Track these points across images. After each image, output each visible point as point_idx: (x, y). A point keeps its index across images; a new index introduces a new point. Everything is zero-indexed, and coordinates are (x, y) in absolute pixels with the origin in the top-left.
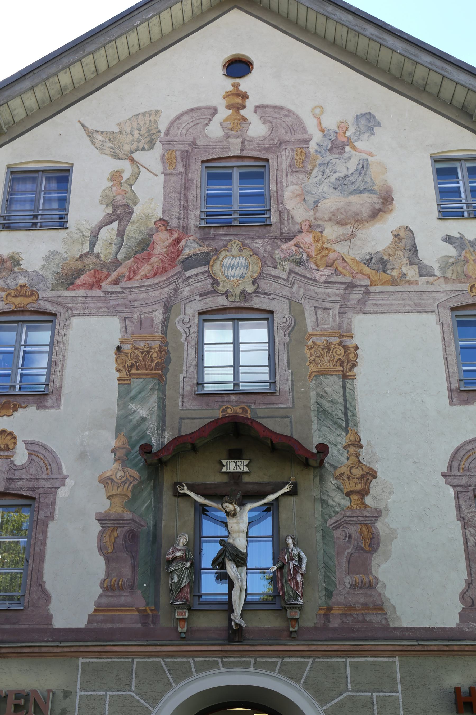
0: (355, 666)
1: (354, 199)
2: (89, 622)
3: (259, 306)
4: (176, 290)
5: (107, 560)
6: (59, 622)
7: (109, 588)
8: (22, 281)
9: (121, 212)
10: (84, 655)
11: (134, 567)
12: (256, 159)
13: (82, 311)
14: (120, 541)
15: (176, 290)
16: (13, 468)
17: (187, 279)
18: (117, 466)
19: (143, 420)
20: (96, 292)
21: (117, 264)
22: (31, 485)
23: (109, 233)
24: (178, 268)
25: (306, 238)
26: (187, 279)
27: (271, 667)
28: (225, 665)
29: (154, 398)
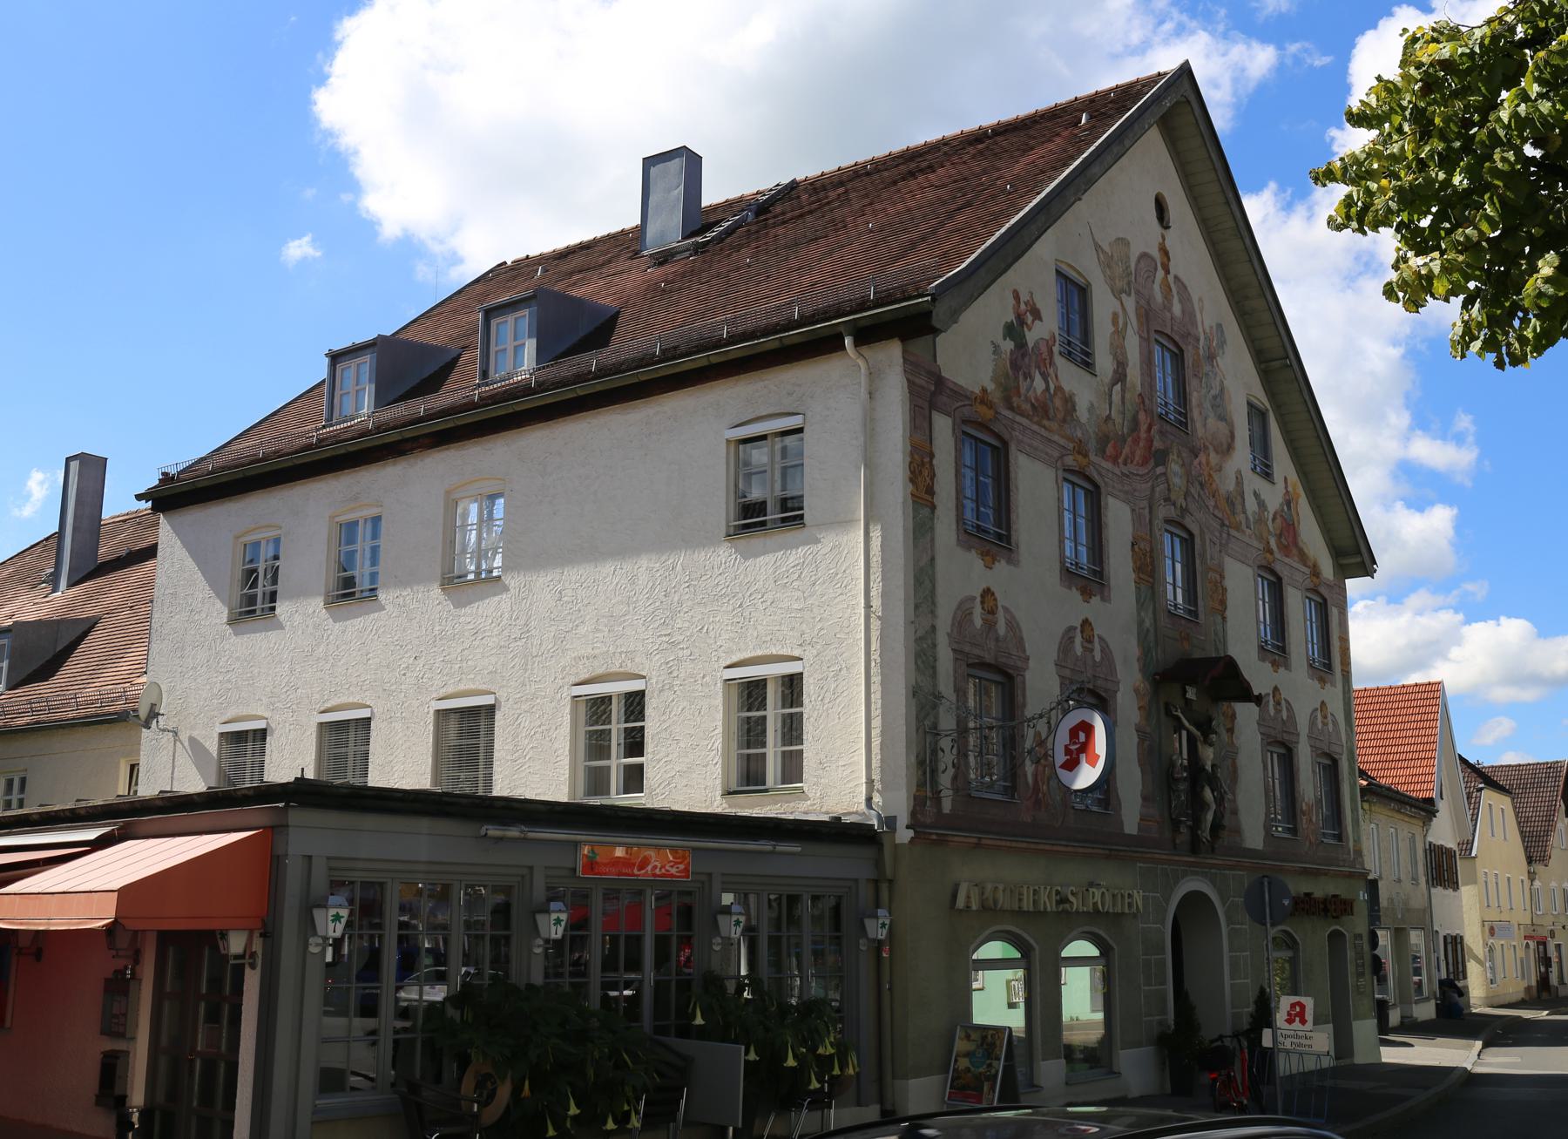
4: (1153, 488)
8: (1079, 434)
24: (1152, 463)
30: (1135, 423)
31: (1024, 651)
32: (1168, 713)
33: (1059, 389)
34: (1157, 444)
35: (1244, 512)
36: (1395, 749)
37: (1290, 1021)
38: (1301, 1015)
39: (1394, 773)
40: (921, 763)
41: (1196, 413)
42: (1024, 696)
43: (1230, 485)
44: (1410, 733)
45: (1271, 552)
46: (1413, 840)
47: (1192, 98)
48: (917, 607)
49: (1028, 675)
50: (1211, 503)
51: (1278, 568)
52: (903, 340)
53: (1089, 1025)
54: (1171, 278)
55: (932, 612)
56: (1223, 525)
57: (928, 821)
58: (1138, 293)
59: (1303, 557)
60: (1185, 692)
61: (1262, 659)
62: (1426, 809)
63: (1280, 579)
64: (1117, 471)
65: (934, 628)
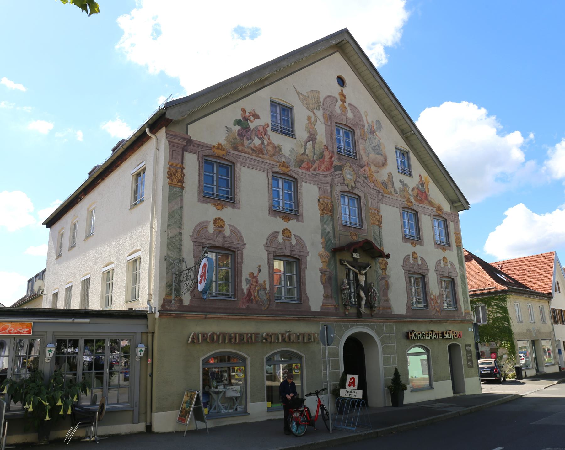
0: (386, 325)
1: (377, 156)
2: (321, 309)
3: (356, 193)
4: (333, 179)
5: (324, 286)
6: (313, 309)
7: (325, 297)
8: (284, 159)
9: (312, 138)
10: (323, 321)
11: (331, 290)
12: (350, 128)
13: (362, 182)
14: (327, 280)
15: (333, 179)
16: (292, 246)
17: (336, 175)
18: (323, 250)
19: (329, 232)
20: (308, 173)
21: (314, 162)
22: (298, 253)
23: (310, 145)
24: (333, 170)
25: (366, 168)
26: (336, 175)
27: (367, 326)
28: (357, 325)
29: (331, 224)
30: (322, 156)
31: (243, 241)
32: (341, 263)
33: (270, 143)
34: (336, 163)
35: (393, 187)
36: (538, 276)
37: (350, 385)
38: (353, 383)
39: (538, 285)
40: (169, 286)
41: (362, 152)
42: (242, 258)
43: (385, 178)
44: (543, 270)
45: (411, 202)
46: (541, 309)
47: (350, 41)
48: (169, 225)
49: (245, 251)
50: (372, 185)
51: (415, 208)
52: (166, 127)
53: (424, 379)
54: (346, 105)
55: (180, 227)
56: (379, 192)
57: (173, 309)
58: (324, 109)
59: (431, 204)
60: (353, 255)
61: (406, 242)
62: (549, 296)
63: (417, 212)
64: (309, 173)
65: (181, 234)
